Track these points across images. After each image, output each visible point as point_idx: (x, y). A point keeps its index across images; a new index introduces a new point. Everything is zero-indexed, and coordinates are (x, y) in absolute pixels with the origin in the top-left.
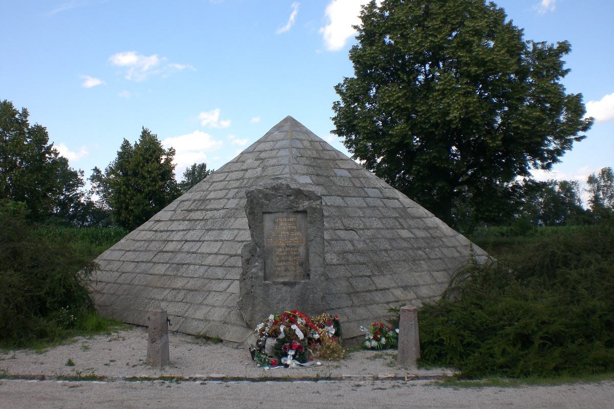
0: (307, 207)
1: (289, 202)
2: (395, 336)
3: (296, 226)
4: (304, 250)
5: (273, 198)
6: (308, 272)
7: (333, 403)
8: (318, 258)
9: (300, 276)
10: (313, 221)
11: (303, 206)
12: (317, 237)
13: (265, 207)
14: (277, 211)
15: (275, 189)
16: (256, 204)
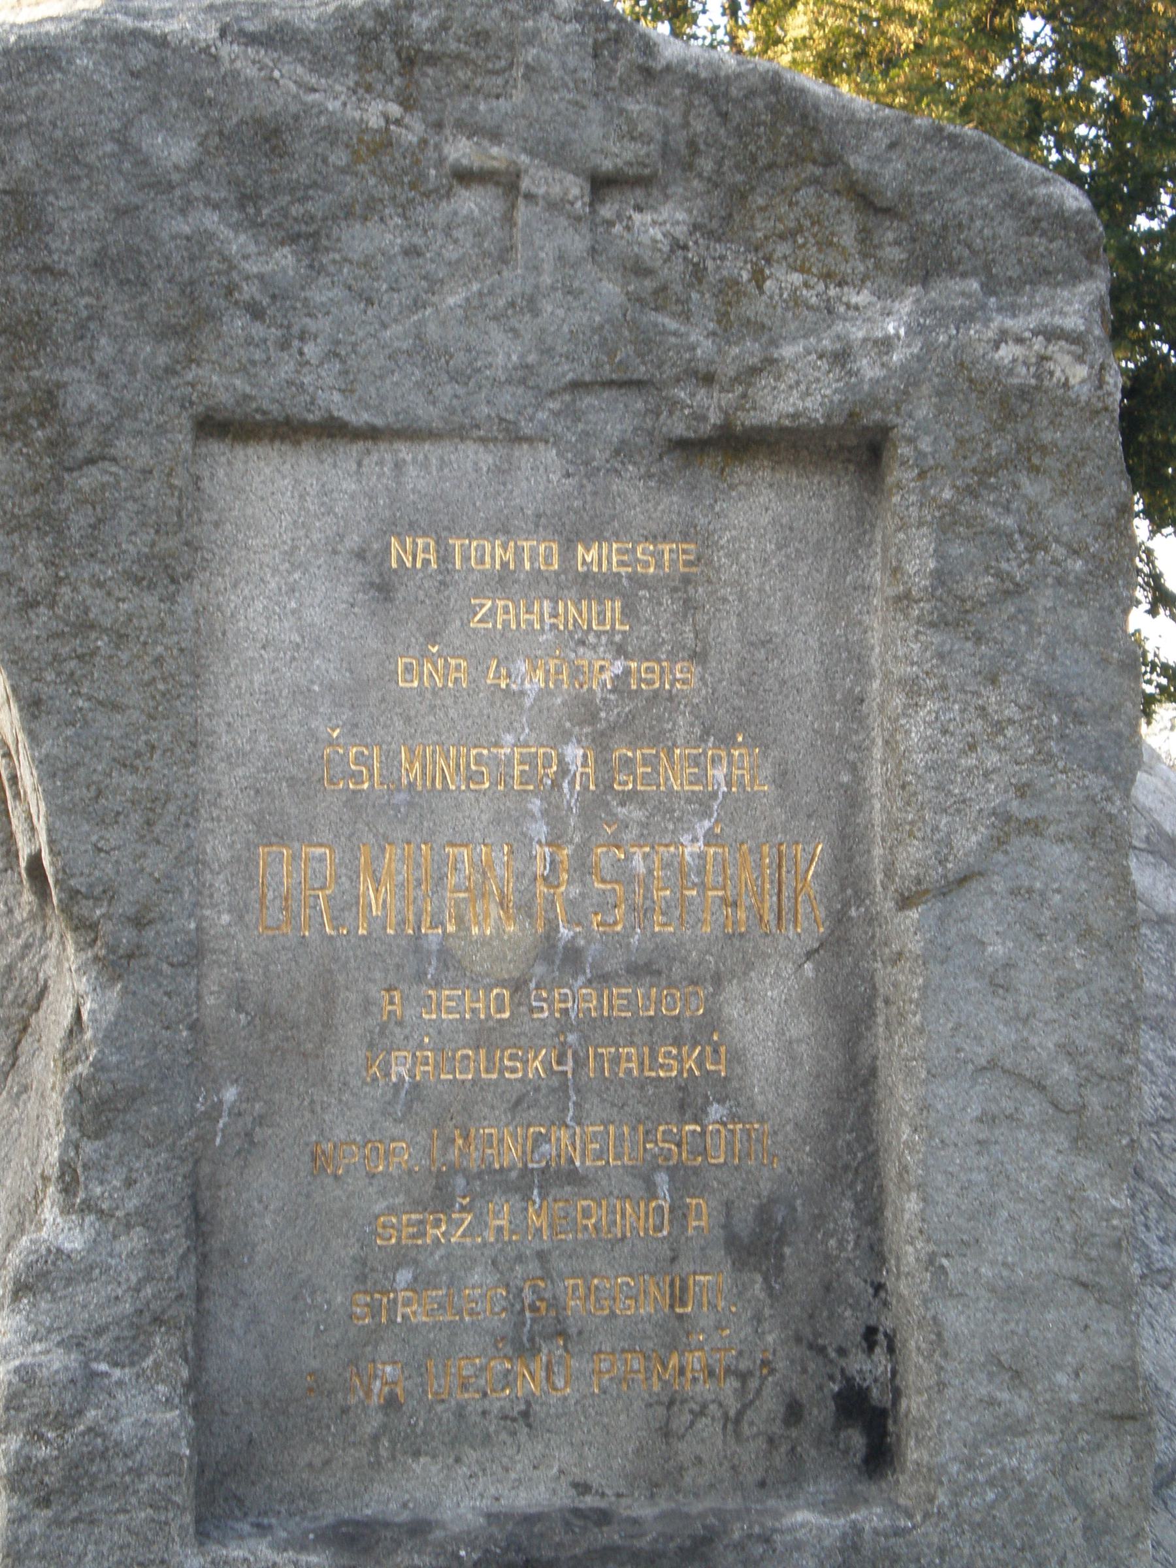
0: (911, 376)
1: (611, 290)
2: (988, 1417)
3: (698, 656)
4: (801, 1027)
5: (370, 209)
6: (858, 1364)
7: (302, 241)
8: (1051, 1161)
9: (734, 1423)
10: (982, 585)
11: (841, 357)
12: (1034, 827)
13: (238, 324)
14: (427, 413)
15: (563, 1333)
16: (98, 264)
